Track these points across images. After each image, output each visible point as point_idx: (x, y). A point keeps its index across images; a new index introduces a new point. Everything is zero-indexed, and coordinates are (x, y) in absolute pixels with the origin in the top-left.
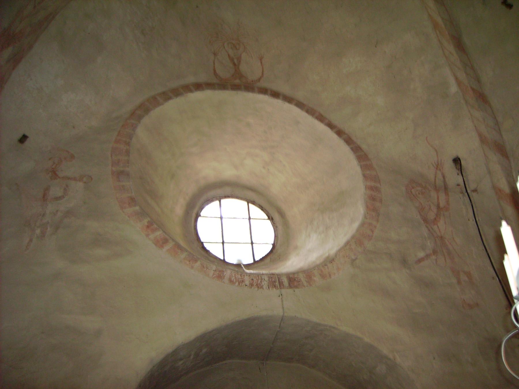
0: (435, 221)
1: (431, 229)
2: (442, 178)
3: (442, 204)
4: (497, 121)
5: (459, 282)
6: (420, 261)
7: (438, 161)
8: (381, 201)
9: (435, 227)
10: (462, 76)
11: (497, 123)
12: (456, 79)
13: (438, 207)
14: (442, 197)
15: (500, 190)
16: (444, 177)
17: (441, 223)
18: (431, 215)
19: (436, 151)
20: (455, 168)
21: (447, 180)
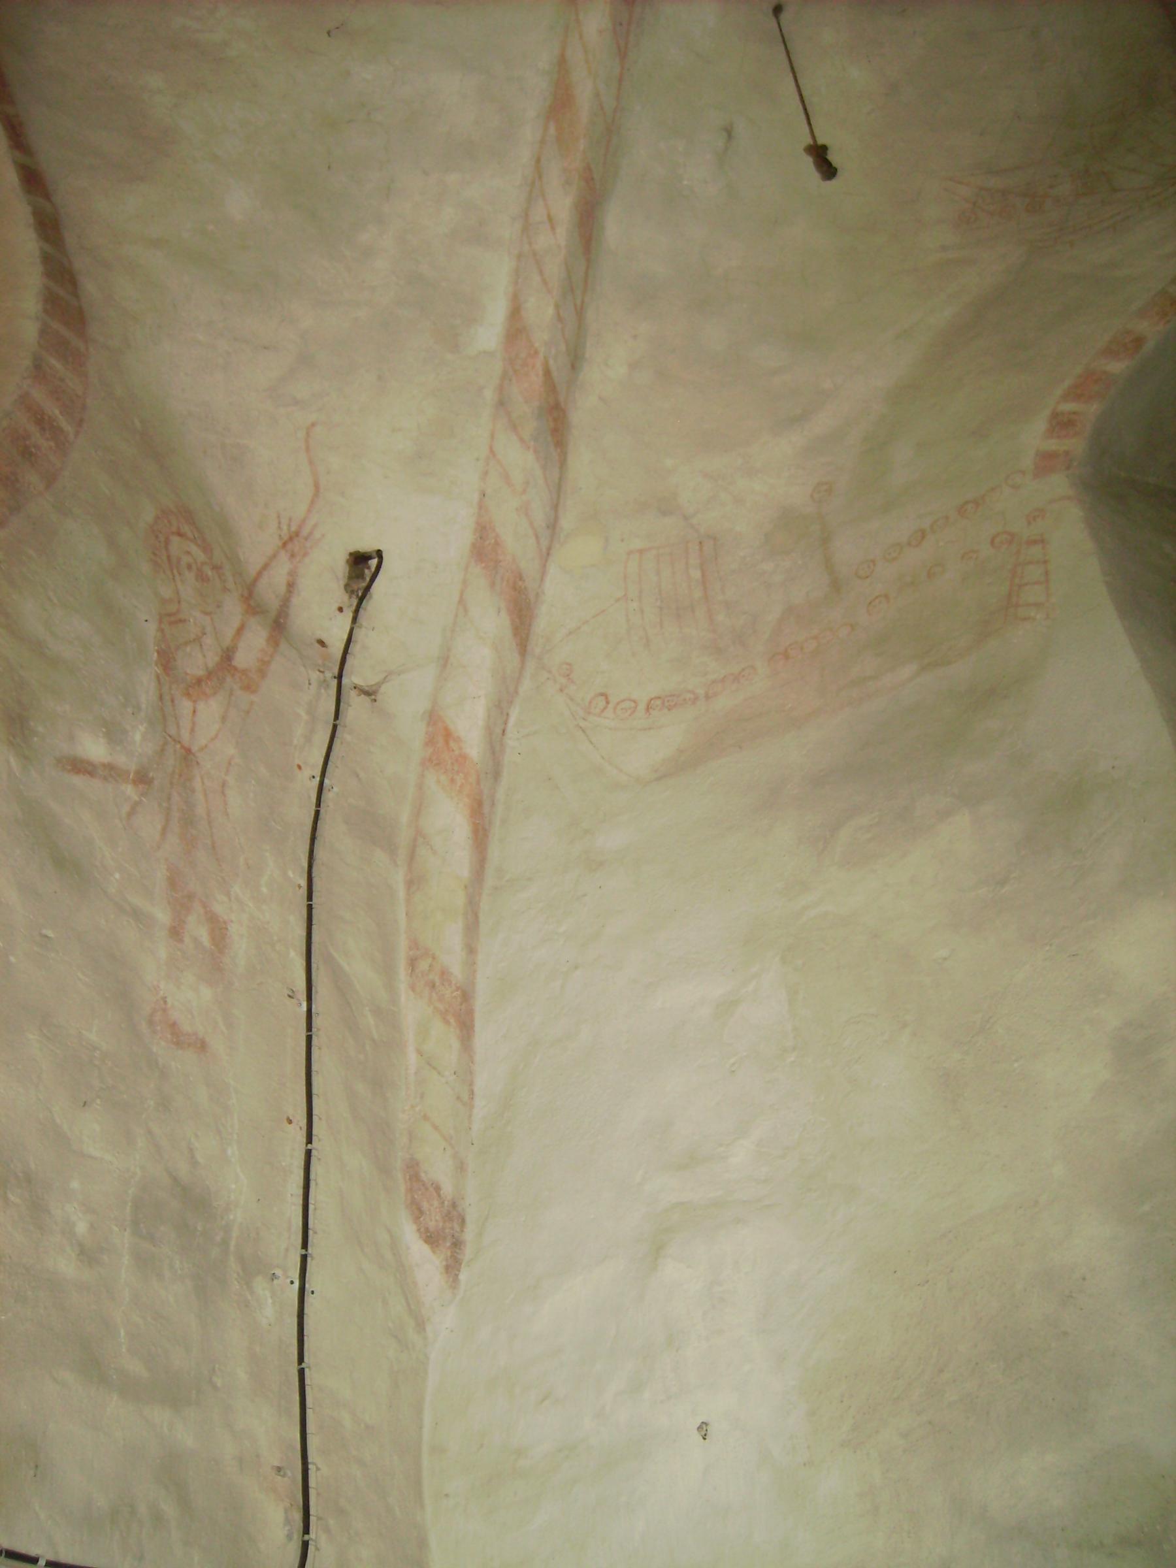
0: (196, 687)
1: (167, 698)
2: (283, 589)
3: (244, 658)
4: (556, 519)
5: (176, 932)
6: (80, 766)
7: (304, 521)
8: (50, 479)
9: (186, 706)
10: (541, 311)
11: (553, 526)
12: (515, 312)
13: (228, 656)
14: (256, 639)
15: (448, 735)
16: (291, 586)
17: (210, 710)
18: (195, 663)
19: (317, 486)
20: (342, 583)
21: (295, 601)
